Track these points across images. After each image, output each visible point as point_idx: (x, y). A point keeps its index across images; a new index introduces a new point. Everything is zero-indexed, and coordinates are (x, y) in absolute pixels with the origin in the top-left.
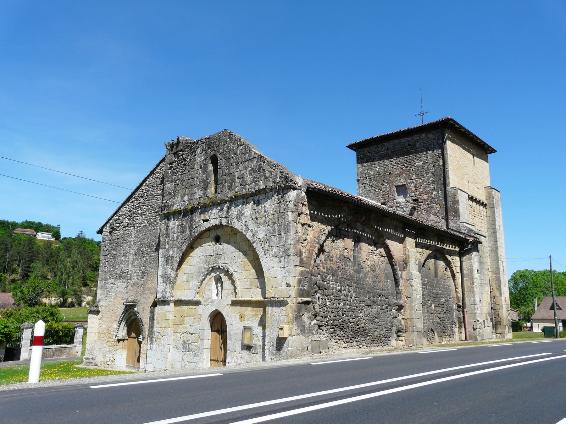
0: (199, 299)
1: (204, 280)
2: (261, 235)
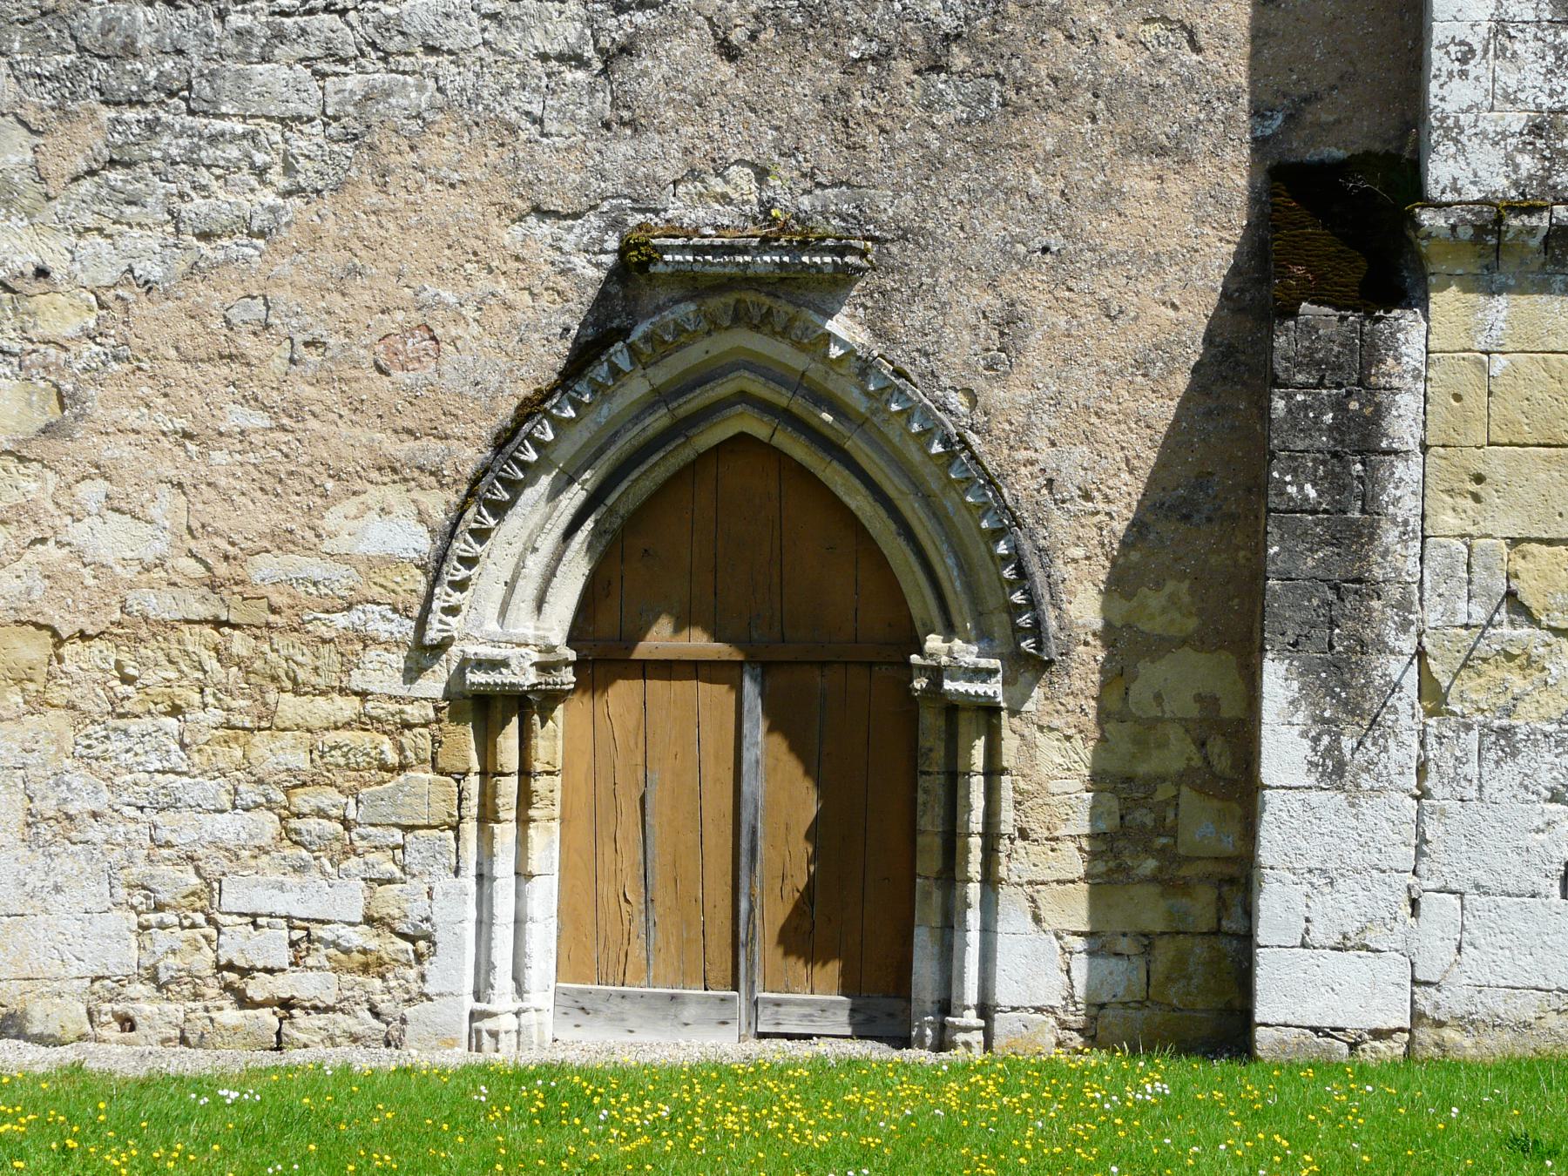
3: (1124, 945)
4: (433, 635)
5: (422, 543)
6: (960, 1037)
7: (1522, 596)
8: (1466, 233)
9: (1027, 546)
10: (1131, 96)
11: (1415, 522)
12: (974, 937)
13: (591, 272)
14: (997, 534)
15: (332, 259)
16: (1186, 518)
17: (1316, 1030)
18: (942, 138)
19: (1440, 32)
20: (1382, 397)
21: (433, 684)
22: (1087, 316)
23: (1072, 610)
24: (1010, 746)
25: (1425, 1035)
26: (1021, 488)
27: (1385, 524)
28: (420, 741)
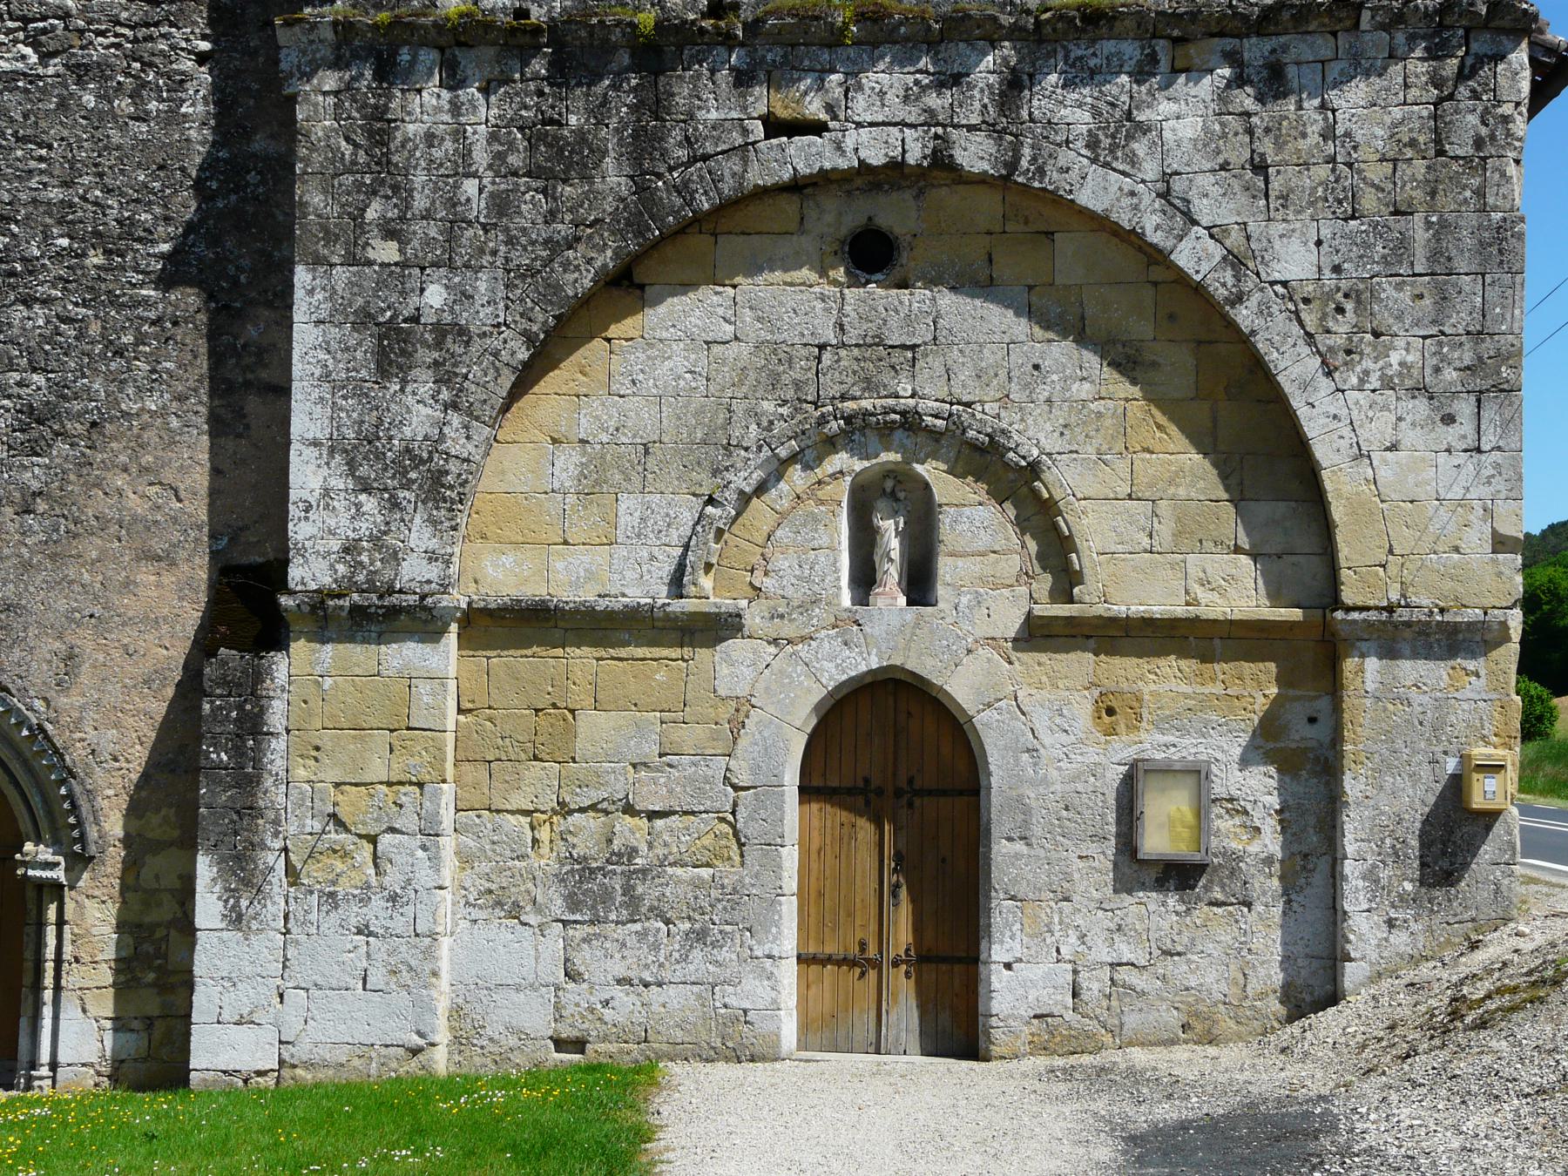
0: (726, 604)
1: (761, 489)
2: (1294, 259)
3: (135, 1024)
6: (36, 1083)
7: (340, 816)
8: (306, 609)
9: (77, 789)
10: (140, 527)
11: (282, 774)
14: (63, 782)
16: (172, 771)
17: (224, 1072)
18: (31, 552)
19: (293, 495)
20: (264, 702)
22: (116, 654)
23: (107, 826)
25: (286, 1073)
26: (76, 755)
27: (266, 775)
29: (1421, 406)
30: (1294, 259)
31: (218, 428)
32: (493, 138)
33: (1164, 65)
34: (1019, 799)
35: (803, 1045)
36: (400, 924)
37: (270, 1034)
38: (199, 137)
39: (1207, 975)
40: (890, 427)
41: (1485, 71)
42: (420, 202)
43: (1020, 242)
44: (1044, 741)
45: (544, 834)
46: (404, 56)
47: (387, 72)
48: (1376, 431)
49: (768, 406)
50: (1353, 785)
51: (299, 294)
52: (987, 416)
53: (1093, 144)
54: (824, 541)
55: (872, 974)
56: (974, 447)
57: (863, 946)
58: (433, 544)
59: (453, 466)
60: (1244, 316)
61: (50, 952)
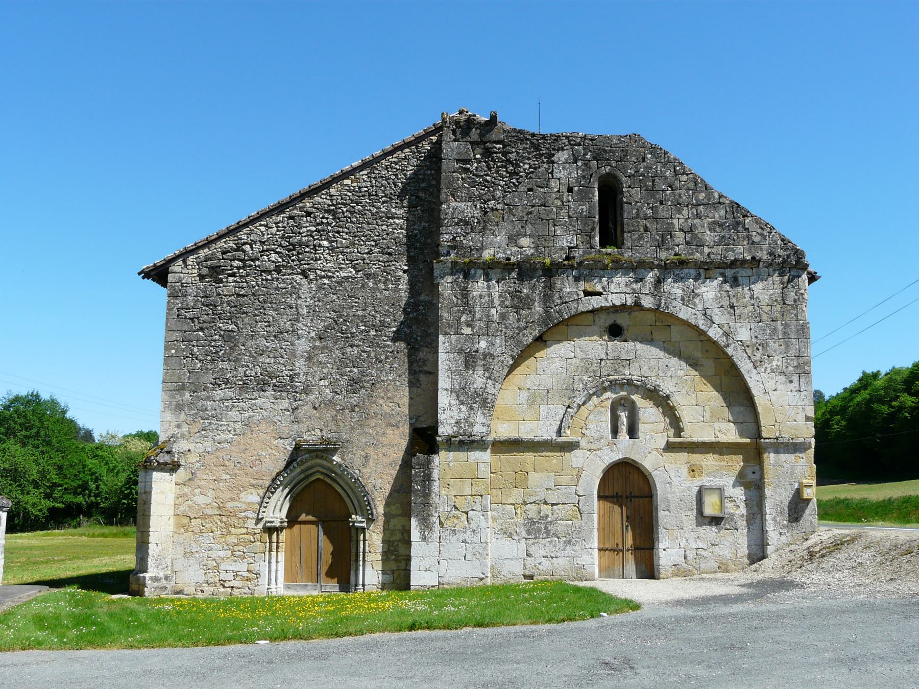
1: (584, 403)
2: (744, 334)
4: (260, 517)
5: (259, 500)
12: (361, 571)
13: (290, 449)
14: (365, 496)
15: (242, 447)
21: (260, 526)
24: (367, 535)
26: (369, 487)
28: (258, 536)
29: (783, 378)
30: (744, 334)
31: (411, 384)
32: (500, 296)
33: (703, 277)
34: (666, 498)
35: (600, 577)
36: (476, 539)
37: (436, 575)
38: (404, 295)
39: (725, 551)
40: (623, 384)
41: (796, 280)
42: (478, 316)
43: (661, 329)
44: (674, 481)
45: (519, 511)
46: (472, 272)
47: (467, 276)
48: (770, 385)
49: (585, 378)
50: (768, 492)
51: (440, 344)
52: (653, 381)
53: (683, 299)
54: (604, 419)
55: (621, 554)
56: (649, 390)
57: (617, 545)
58: (484, 421)
59: (490, 397)
60: (730, 351)
61: (361, 550)
